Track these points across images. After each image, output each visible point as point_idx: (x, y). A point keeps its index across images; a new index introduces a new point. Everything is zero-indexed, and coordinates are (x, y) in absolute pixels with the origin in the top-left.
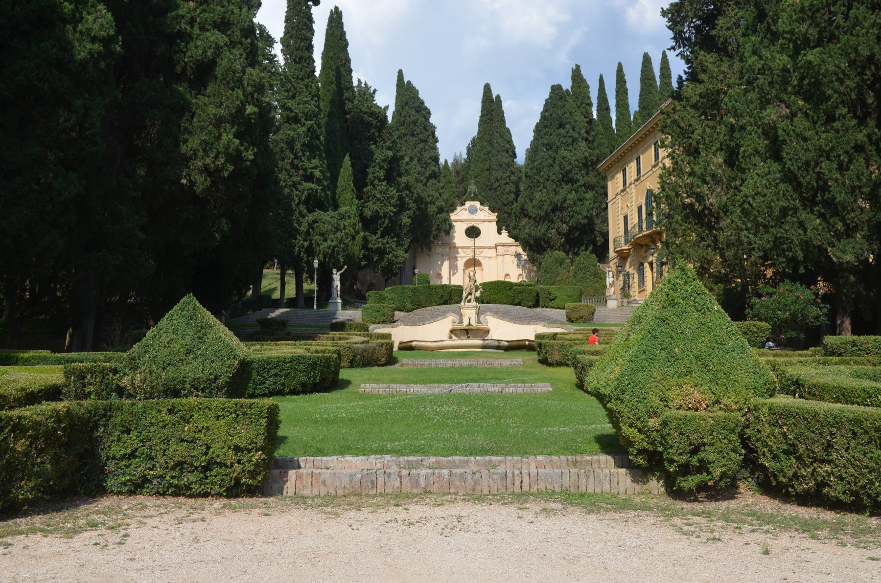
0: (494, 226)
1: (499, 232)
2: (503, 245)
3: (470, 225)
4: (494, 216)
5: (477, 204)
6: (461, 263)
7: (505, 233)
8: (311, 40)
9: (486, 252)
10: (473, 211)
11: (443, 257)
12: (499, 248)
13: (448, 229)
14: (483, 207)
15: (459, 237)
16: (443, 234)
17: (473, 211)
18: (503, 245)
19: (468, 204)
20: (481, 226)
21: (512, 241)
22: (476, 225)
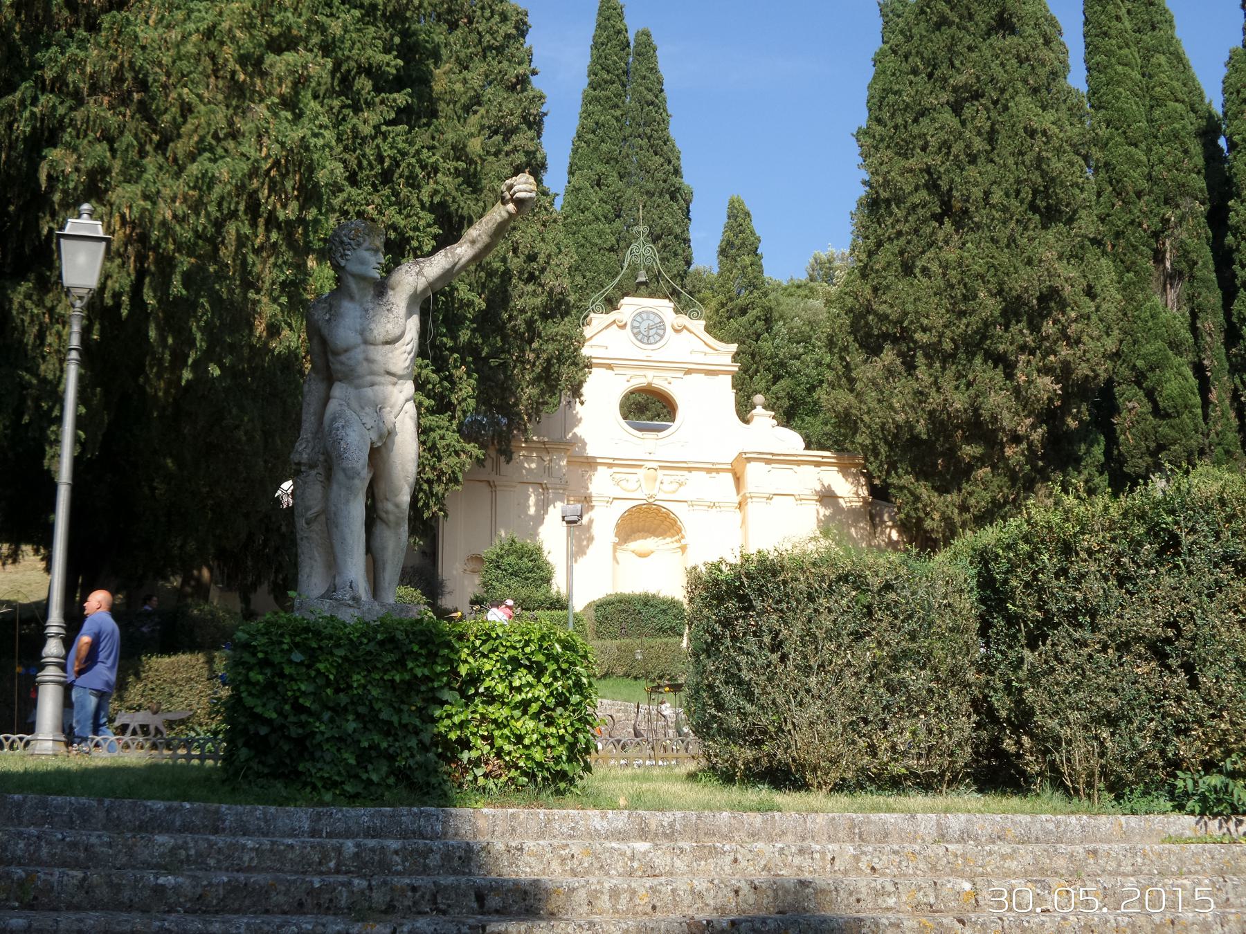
0: (723, 391)
1: (744, 411)
2: (771, 459)
3: (640, 379)
4: (724, 354)
5: (664, 307)
6: (603, 520)
7: (763, 418)
8: (289, 50)
9: (699, 486)
10: (648, 332)
11: (550, 488)
12: (754, 472)
13: (562, 376)
14: (683, 319)
15: (597, 416)
16: (565, 397)
17: (648, 332)
18: (771, 459)
19: (630, 306)
20: (676, 388)
21: (791, 441)
22: (659, 381)
